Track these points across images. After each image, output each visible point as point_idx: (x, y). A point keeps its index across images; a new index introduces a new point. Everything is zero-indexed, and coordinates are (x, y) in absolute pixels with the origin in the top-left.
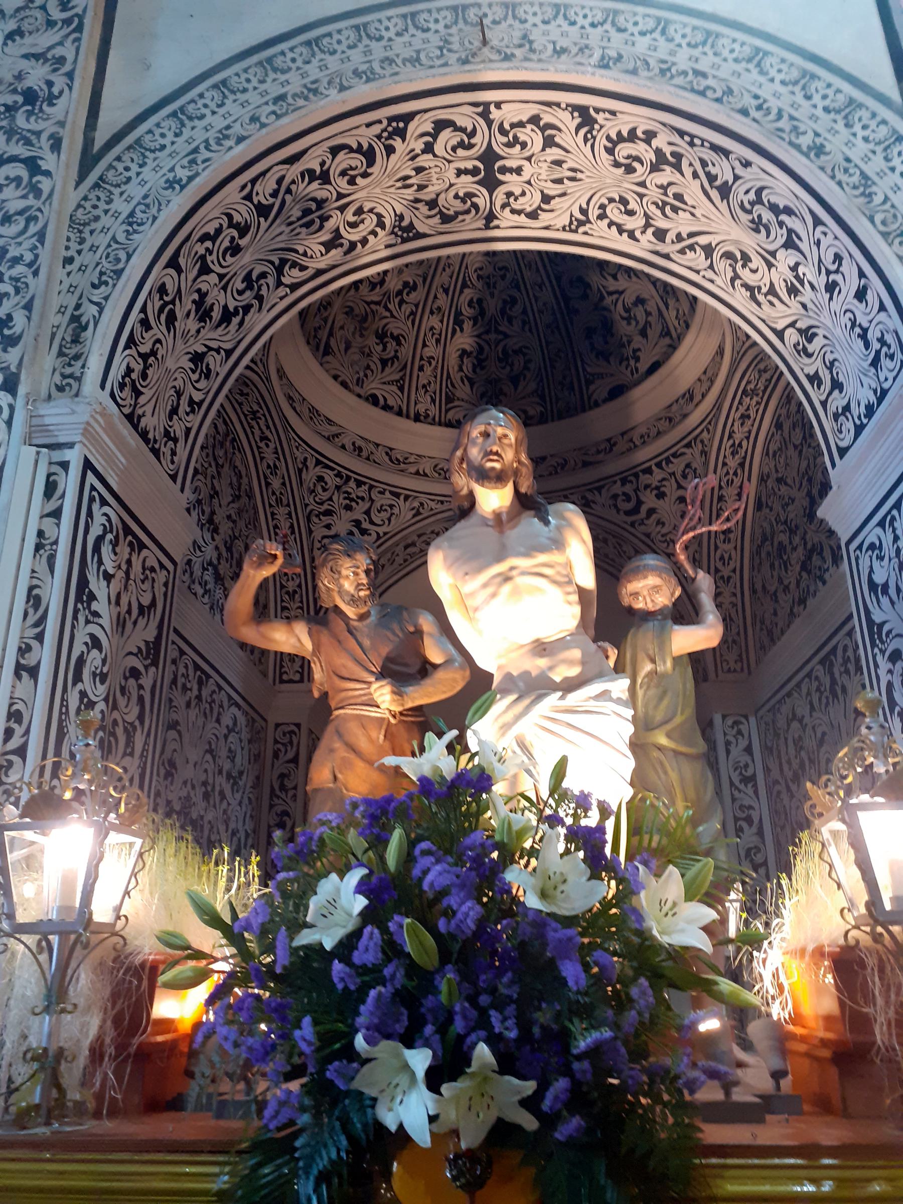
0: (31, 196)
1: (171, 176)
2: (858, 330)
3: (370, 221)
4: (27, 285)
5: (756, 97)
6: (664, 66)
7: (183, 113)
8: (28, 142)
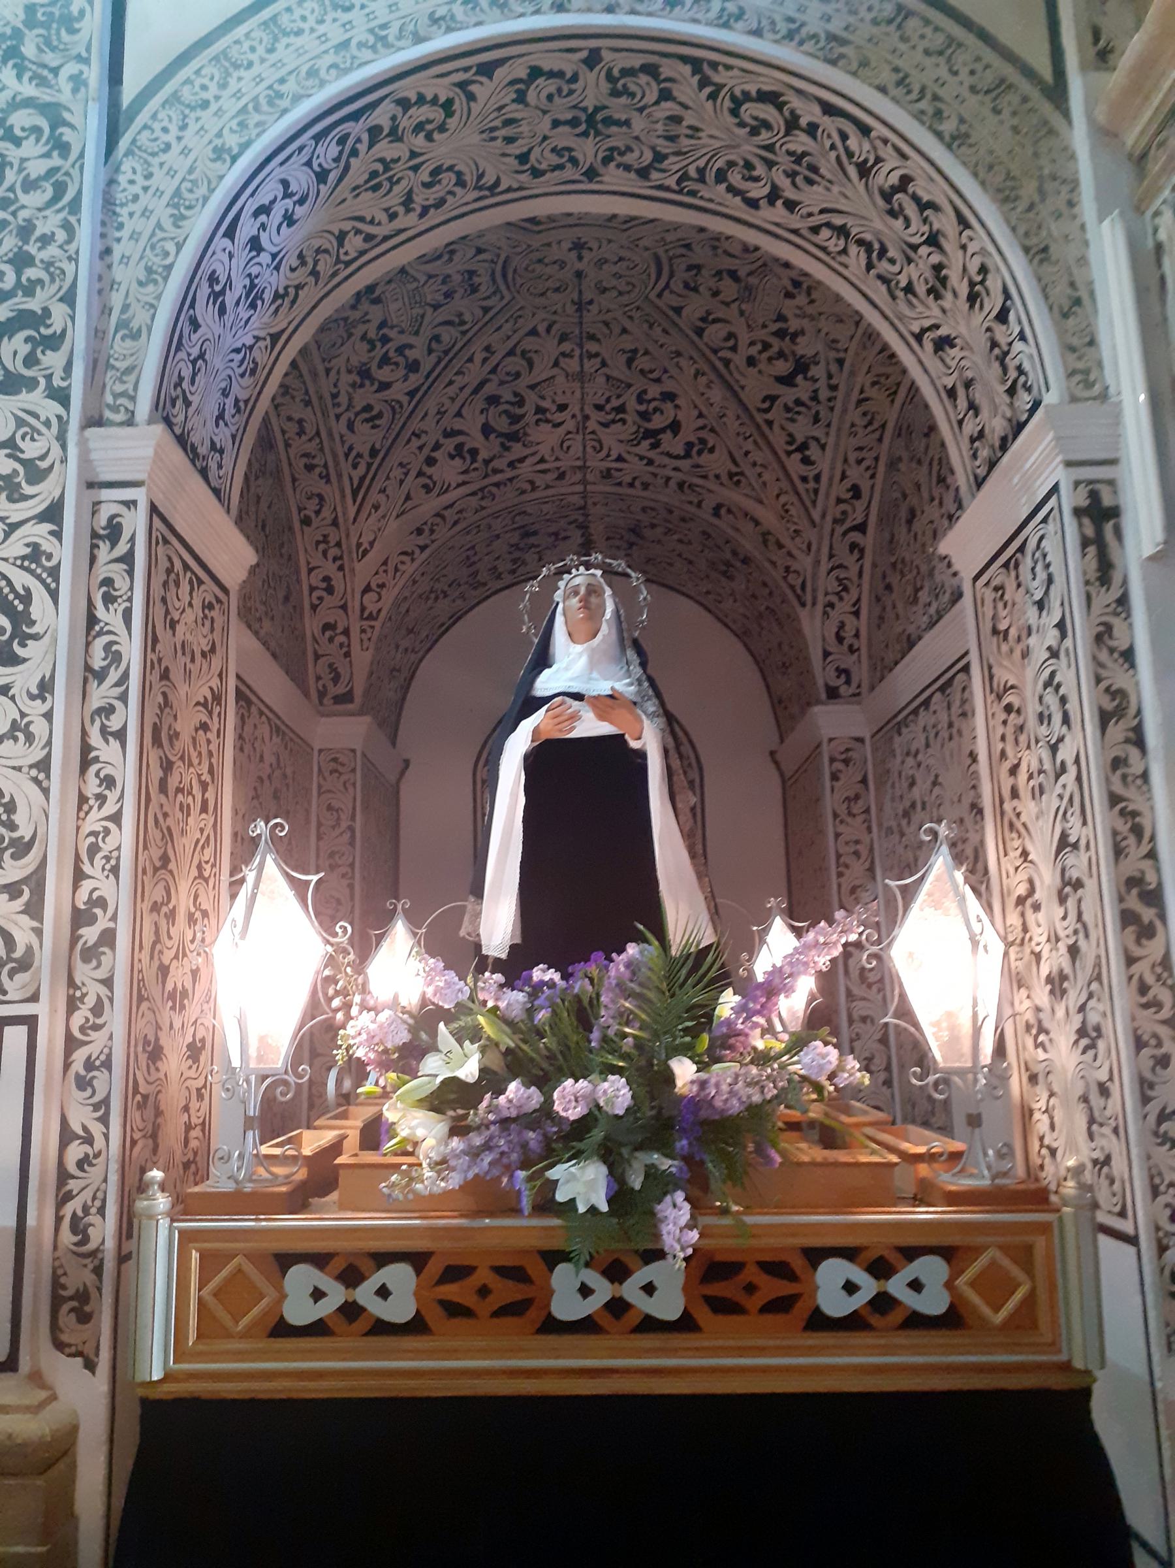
0: (55, 154)
1: (219, 142)
2: (997, 351)
3: (448, 179)
4: (63, 272)
5: (896, 70)
6: (793, 26)
7: (226, 58)
8: (42, 82)
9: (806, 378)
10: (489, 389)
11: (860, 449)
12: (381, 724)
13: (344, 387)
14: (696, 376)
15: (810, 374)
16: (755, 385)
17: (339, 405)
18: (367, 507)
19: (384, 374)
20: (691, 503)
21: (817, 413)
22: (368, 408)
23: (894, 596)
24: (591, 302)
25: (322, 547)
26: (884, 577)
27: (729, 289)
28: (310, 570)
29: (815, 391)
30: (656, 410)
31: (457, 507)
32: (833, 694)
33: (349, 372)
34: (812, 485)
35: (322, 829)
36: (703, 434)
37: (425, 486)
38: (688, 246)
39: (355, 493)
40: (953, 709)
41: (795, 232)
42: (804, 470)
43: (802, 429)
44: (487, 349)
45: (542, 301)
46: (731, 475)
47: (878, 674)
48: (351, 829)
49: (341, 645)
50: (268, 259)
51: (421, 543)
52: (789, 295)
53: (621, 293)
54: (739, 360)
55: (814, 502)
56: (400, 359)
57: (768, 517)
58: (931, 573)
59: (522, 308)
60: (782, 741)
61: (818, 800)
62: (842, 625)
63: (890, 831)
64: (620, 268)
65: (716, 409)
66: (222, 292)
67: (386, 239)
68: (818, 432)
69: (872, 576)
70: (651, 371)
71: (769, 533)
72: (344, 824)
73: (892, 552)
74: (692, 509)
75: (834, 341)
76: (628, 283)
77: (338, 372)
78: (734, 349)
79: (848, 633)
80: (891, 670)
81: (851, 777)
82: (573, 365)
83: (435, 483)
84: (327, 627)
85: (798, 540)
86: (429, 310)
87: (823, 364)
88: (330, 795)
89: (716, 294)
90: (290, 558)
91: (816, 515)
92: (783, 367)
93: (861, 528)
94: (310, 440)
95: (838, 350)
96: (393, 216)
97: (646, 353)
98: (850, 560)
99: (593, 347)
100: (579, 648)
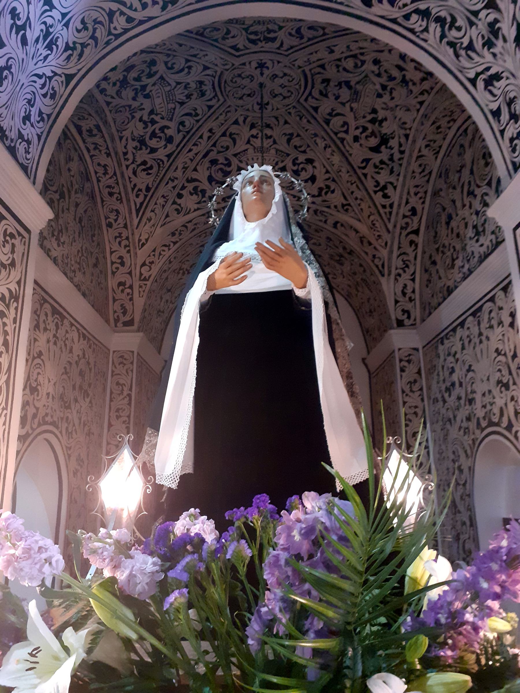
9: (386, 148)
10: (212, 155)
11: (417, 186)
12: (152, 340)
13: (130, 148)
14: (325, 148)
15: (389, 145)
16: (358, 153)
17: (127, 159)
18: (144, 220)
19: (153, 143)
20: (321, 221)
21: (392, 168)
22: (144, 163)
23: (438, 267)
24: (267, 104)
25: (118, 240)
26: (431, 257)
27: (345, 94)
28: (112, 253)
29: (392, 155)
30: (303, 169)
31: (194, 222)
32: (400, 324)
33: (133, 140)
34: (388, 210)
35: (113, 396)
36: (328, 183)
37: (177, 210)
38: (322, 66)
39: (138, 211)
40: (482, 326)
41: (394, 21)
42: (384, 201)
43: (383, 178)
44: (210, 131)
45: (240, 102)
46: (343, 206)
47: (427, 312)
48: (129, 395)
49: (128, 294)
50: (58, 17)
51: (174, 241)
52: (380, 96)
53: (285, 98)
54: (349, 138)
55: (389, 220)
56: (162, 135)
57: (363, 229)
58: (464, 249)
59: (229, 106)
60: (369, 352)
61: (392, 383)
62: (405, 286)
63: (436, 400)
64: (284, 81)
65: (336, 168)
66: (23, 27)
67: (141, 22)
68: (392, 179)
69: (423, 258)
70: (300, 147)
71: (364, 237)
72: (125, 393)
73: (435, 242)
74: (321, 224)
75: (405, 123)
76: (289, 91)
77: (127, 140)
78: (347, 132)
79: (409, 290)
80: (436, 309)
81: (412, 369)
82: (257, 143)
83: (182, 208)
84: (120, 284)
85: (380, 240)
86: (178, 105)
87: (396, 138)
88: (119, 376)
89: (337, 98)
90: (98, 244)
91: (390, 226)
92: (373, 142)
93: (416, 232)
94: (110, 178)
95: (406, 129)
96: (144, 6)
97: (298, 135)
98: (410, 250)
99: (268, 132)
100: (253, 225)
